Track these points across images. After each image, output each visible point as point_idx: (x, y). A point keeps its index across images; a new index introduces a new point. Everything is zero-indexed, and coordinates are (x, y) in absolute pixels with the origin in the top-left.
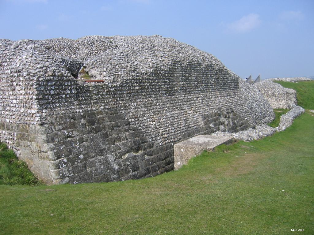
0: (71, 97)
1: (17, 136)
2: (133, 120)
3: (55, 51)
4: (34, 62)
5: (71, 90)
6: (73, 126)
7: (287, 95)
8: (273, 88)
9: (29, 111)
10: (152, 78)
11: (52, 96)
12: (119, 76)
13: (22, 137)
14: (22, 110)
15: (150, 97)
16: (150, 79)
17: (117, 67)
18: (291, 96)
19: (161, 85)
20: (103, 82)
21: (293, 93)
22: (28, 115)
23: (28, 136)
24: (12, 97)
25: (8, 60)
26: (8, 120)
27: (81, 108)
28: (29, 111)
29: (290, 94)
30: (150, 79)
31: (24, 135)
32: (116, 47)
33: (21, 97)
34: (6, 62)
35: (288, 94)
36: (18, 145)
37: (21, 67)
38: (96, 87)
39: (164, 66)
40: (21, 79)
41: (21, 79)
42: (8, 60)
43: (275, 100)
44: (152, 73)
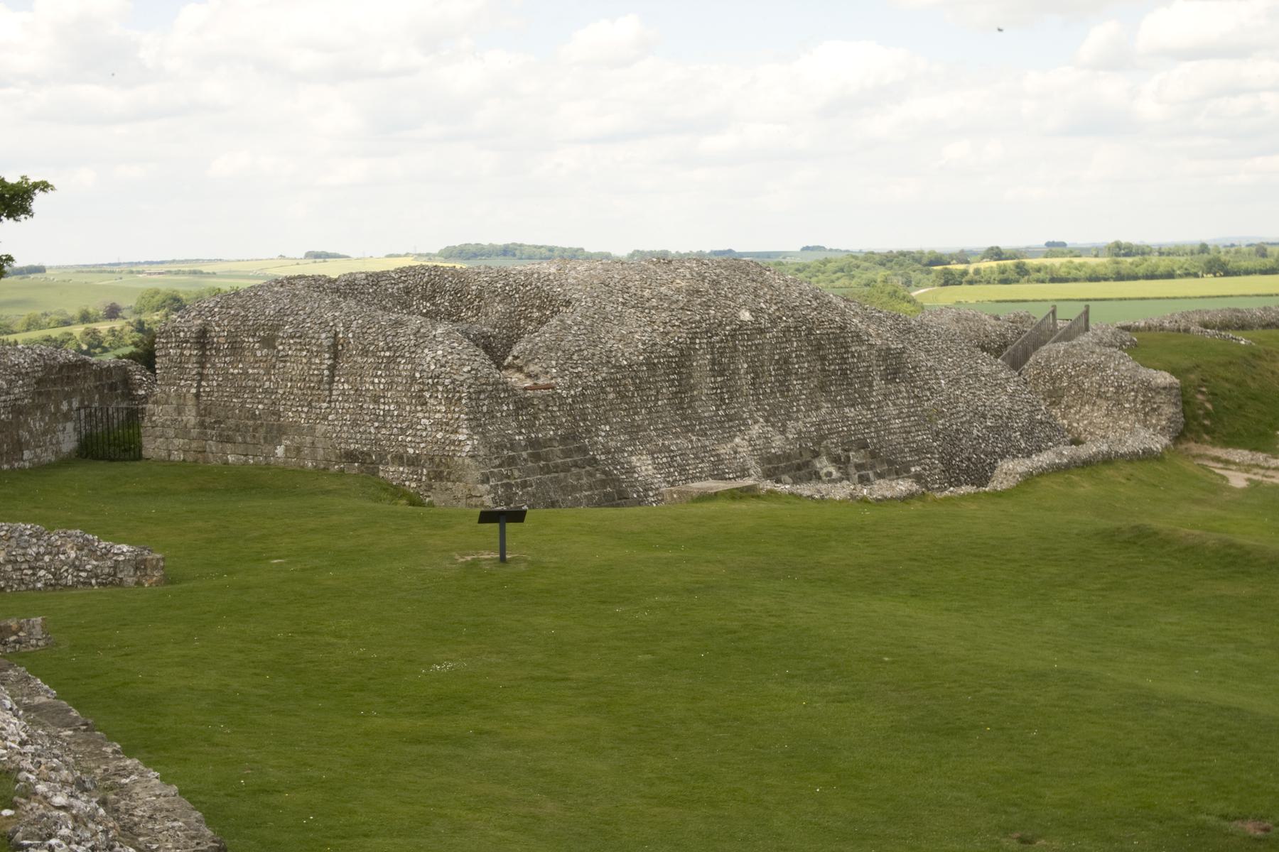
0: (508, 415)
1: (428, 475)
2: (603, 457)
3: (422, 298)
4: (458, 363)
5: (508, 405)
6: (511, 461)
7: (1144, 396)
8: (1097, 368)
9: (453, 437)
10: (640, 374)
11: (484, 414)
12: (579, 376)
13: (438, 476)
14: (439, 435)
15: (635, 414)
16: (637, 377)
17: (575, 357)
18: (1158, 399)
19: (662, 387)
20: (553, 388)
21: (1165, 388)
22: (453, 443)
23: (449, 473)
24: (420, 415)
25: (407, 355)
26: (411, 451)
27: (521, 433)
28: (453, 437)
29: (1157, 390)
30: (637, 377)
31: (442, 472)
32: (568, 303)
33: (438, 415)
34: (403, 357)
35: (1149, 388)
36: (430, 488)
37: (438, 371)
38: (543, 398)
39: (668, 345)
40: (440, 388)
41: (440, 388)
42: (407, 355)
43: (1104, 411)
44: (642, 364)
